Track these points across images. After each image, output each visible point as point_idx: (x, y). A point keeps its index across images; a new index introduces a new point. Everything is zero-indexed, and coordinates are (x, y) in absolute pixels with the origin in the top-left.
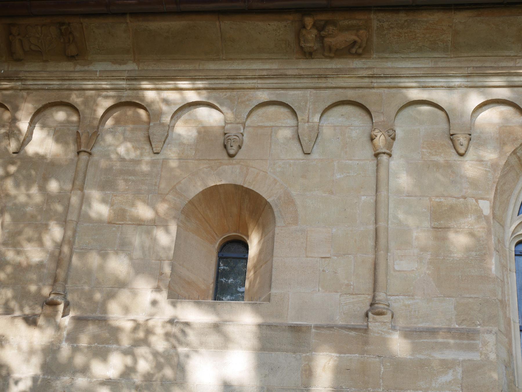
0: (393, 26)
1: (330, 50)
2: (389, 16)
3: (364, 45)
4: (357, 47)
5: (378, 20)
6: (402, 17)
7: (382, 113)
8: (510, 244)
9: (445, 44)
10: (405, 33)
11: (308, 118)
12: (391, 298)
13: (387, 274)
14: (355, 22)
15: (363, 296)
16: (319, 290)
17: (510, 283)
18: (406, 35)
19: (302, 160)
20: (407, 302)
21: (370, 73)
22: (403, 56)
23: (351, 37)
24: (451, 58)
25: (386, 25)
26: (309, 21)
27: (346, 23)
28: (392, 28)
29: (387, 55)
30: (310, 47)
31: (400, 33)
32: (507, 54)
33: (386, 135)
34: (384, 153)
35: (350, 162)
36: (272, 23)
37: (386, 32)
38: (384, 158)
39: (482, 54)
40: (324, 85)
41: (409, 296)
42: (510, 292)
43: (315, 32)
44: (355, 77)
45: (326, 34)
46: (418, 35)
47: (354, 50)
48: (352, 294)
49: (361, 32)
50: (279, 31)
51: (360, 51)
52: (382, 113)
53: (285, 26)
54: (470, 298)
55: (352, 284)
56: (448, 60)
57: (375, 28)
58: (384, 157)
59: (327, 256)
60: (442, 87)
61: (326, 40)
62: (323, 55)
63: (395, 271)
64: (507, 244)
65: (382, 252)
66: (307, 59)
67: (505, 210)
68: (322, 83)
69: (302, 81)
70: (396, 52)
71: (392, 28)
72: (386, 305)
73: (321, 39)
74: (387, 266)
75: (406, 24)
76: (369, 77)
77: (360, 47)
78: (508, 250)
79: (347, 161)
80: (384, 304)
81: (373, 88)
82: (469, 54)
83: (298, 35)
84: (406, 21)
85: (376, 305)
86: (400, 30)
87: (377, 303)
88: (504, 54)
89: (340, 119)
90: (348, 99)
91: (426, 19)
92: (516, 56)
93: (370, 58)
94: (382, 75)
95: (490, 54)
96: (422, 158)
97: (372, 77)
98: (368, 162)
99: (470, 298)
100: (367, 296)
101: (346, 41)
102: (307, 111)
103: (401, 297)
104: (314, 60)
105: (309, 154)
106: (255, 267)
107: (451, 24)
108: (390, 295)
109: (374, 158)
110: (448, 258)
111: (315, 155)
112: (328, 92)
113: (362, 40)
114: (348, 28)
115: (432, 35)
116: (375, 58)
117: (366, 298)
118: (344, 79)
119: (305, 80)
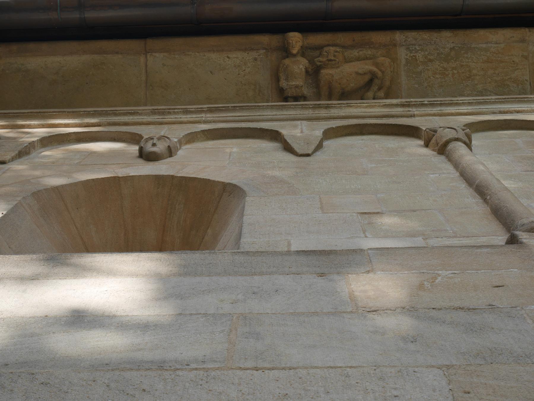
0: (432, 57)
2: (425, 35)
3: (388, 83)
5: (408, 49)
6: (447, 39)
9: (520, 87)
10: (453, 68)
14: (369, 52)
18: (455, 72)
25: (420, 56)
28: (431, 61)
30: (297, 87)
31: (445, 69)
36: (233, 55)
37: (421, 68)
45: (324, 59)
46: (474, 72)
50: (244, 68)
53: (255, 59)
57: (403, 62)
61: (325, 72)
71: (431, 61)
73: (314, 73)
75: (453, 53)
77: (380, 89)
86: (445, 65)
91: (484, 46)
101: (357, 73)
105: (308, 155)
106: (67, 150)
107: (525, 54)
113: (383, 72)
115: (497, 72)
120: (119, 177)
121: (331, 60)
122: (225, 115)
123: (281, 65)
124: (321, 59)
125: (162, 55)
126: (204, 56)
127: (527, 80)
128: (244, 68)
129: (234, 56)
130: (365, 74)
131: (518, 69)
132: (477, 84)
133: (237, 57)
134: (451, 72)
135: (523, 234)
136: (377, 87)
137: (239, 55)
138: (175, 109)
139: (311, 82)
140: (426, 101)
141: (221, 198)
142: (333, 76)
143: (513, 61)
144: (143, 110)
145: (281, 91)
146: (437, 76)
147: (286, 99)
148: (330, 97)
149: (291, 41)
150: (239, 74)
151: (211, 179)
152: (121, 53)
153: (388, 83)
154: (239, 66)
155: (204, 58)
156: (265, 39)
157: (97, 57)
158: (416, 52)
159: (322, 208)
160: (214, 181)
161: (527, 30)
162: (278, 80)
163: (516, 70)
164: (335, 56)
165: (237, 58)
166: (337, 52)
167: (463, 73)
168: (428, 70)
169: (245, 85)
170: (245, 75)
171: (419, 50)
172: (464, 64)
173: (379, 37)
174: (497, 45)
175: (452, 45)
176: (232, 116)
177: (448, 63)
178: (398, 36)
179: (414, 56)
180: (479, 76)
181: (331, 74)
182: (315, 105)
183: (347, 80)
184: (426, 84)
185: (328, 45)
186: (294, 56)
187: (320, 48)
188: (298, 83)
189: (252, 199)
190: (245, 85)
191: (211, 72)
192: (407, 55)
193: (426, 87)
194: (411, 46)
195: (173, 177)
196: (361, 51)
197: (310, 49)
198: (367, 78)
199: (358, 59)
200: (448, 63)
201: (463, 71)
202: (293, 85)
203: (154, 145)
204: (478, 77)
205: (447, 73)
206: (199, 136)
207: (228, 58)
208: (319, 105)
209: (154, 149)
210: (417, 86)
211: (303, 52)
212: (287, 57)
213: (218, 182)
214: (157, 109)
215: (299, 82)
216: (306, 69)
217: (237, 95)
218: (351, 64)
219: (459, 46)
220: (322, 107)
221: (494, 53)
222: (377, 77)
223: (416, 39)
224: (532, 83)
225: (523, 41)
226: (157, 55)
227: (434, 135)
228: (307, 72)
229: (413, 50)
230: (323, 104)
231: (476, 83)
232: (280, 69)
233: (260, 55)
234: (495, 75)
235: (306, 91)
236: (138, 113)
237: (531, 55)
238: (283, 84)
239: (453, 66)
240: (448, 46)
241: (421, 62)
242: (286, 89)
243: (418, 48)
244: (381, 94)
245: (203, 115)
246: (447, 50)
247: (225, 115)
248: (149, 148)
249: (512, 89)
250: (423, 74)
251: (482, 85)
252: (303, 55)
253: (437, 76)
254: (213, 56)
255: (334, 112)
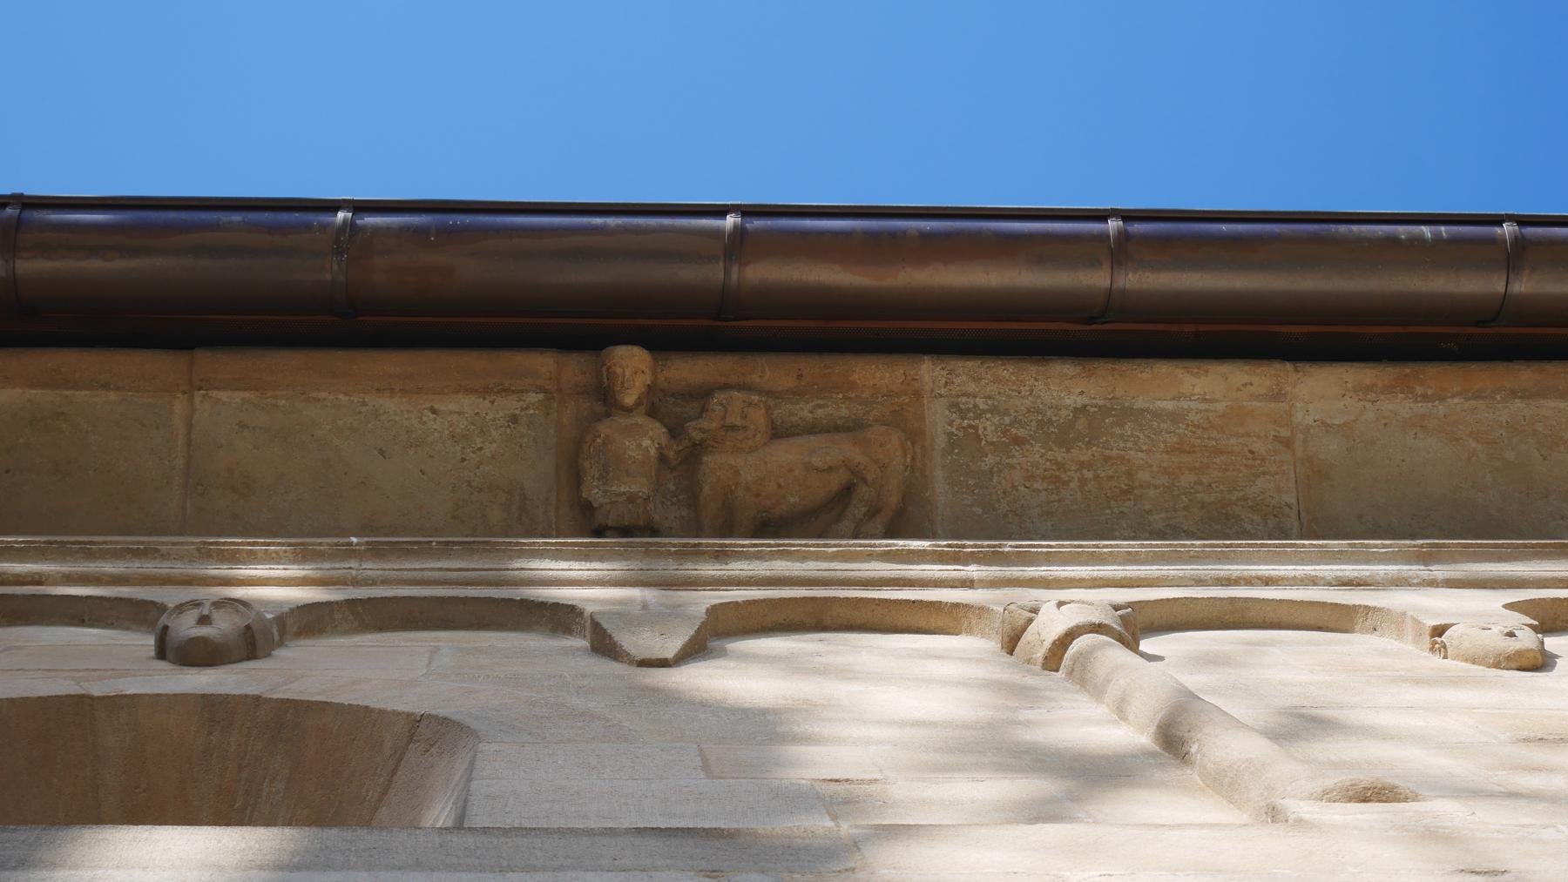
0: (1022, 433)
5: (954, 406)
10: (1082, 465)
18: (1089, 475)
30: (632, 499)
31: (1061, 466)
36: (448, 405)
37: (990, 460)
46: (1143, 476)
50: (478, 442)
53: (514, 419)
57: (941, 442)
71: (1018, 441)
73: (684, 461)
86: (1060, 454)
91: (1169, 405)
101: (809, 467)
107: (1285, 433)
120: (90, 697)
121: (733, 428)
122: (417, 565)
123: (589, 438)
124: (705, 424)
125: (239, 396)
126: (364, 404)
127: (1289, 506)
128: (478, 442)
129: (452, 407)
130: (830, 469)
131: (1264, 473)
133: (460, 409)
134: (1076, 476)
135: (1301, 804)
136: (864, 510)
137: (467, 403)
138: (268, 544)
140: (1008, 546)
141: (400, 760)
142: (737, 472)
143: (1252, 452)
144: (174, 544)
145: (587, 508)
147: (598, 533)
148: (728, 530)
149: (619, 370)
150: (463, 460)
151: (372, 705)
152: (117, 389)
154: (464, 437)
155: (364, 409)
156: (543, 363)
157: (45, 397)
158: (979, 417)
159: (706, 767)
160: (382, 712)
161: (1289, 366)
162: (577, 478)
163: (1257, 476)
165: (459, 413)
167: (1110, 478)
168: (1012, 467)
169: (480, 490)
170: (481, 463)
171: (985, 412)
172: (1114, 453)
174: (1204, 406)
175: (1080, 401)
176: (440, 569)
177: (1068, 451)
178: (929, 371)
179: (970, 426)
180: (1156, 487)
182: (685, 545)
183: (779, 485)
184: (1004, 507)
185: (726, 387)
186: (629, 410)
187: (703, 394)
188: (635, 488)
189: (497, 747)
190: (480, 490)
191: (381, 452)
192: (951, 423)
193: (1005, 515)
194: (964, 399)
195: (257, 699)
196: (819, 406)
197: (673, 395)
198: (836, 481)
199: (812, 429)
200: (1068, 451)
201: (1110, 473)
202: (620, 495)
203: (204, 620)
204: (1152, 492)
205: (1065, 477)
206: (338, 616)
207: (434, 411)
208: (695, 545)
209: (204, 631)
210: (979, 511)
211: (654, 404)
212: (608, 415)
213: (395, 713)
214: (217, 544)
216: (660, 449)
217: (454, 517)
218: (792, 440)
219: (1101, 403)
220: (703, 553)
222: (864, 480)
223: (977, 380)
224: (1303, 514)
225: (1277, 396)
226: (224, 396)
227: (1030, 621)
228: (662, 459)
229: (968, 410)
230: (708, 545)
231: (1147, 507)
232: (586, 448)
233: (527, 408)
234: (1200, 488)
236: (157, 550)
237: (1300, 436)
238: (594, 492)
239: (1082, 459)
240: (1068, 402)
241: (992, 443)
242: (601, 506)
243: (982, 406)
244: (879, 523)
245: (354, 564)
247: (417, 565)
248: (186, 627)
250: (995, 479)
251: (1163, 515)
252: (653, 413)
253: (1037, 485)
254: (391, 404)
255: (738, 568)
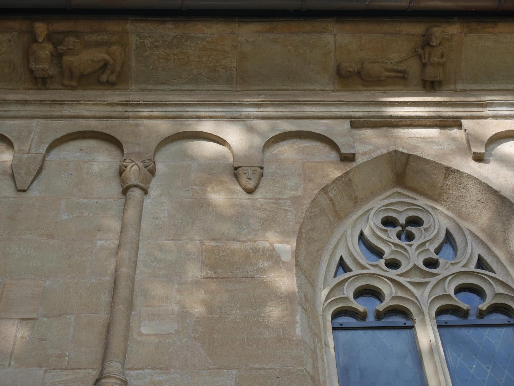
0: (157, 44)
1: (71, 76)
3: (118, 69)
4: (109, 72)
5: (138, 35)
6: (169, 30)
7: (138, 144)
8: (325, 310)
10: (175, 55)
11: (30, 149)
12: (132, 372)
13: (126, 338)
14: (106, 37)
15: (83, 370)
16: (10, 365)
17: (325, 360)
18: (176, 57)
19: (13, 198)
20: (156, 379)
21: (125, 99)
22: (172, 88)
23: (99, 55)
24: (237, 91)
25: (148, 42)
26: (41, 28)
27: (94, 38)
28: (156, 47)
29: (150, 87)
30: (43, 70)
31: (168, 55)
32: (312, 88)
33: (142, 168)
34: (136, 186)
35: (85, 200)
37: (148, 53)
38: (136, 193)
39: (278, 88)
40: (58, 114)
41: (161, 369)
42: (327, 372)
43: (49, 47)
44: (103, 104)
45: (65, 48)
47: (105, 77)
48: (66, 369)
49: (114, 48)
51: (113, 78)
52: (138, 144)
54: (262, 369)
55: (67, 354)
56: (233, 93)
57: (134, 47)
58: (136, 193)
59: (32, 317)
60: (224, 117)
61: (65, 58)
62: (63, 84)
63: (140, 334)
64: (321, 309)
65: (121, 306)
66: (39, 89)
67: (316, 264)
68: (56, 111)
69: (27, 108)
70: (163, 83)
71: (156, 47)
72: (121, 380)
73: (58, 57)
74: (128, 327)
75: (175, 41)
76: (122, 104)
77: (112, 72)
78: (321, 317)
79: (81, 200)
80: (116, 378)
81: (128, 118)
82: (261, 87)
83: (27, 55)
84: (175, 37)
85: (104, 380)
86: (168, 51)
87: (105, 377)
88: (307, 88)
89: (77, 154)
90: (91, 129)
91: (201, 35)
92: (323, 90)
93: (127, 89)
94: (141, 102)
95: (288, 88)
96: (192, 195)
97: (127, 105)
98: (113, 200)
99: (262, 369)
100: (90, 371)
101: (93, 61)
102: (30, 142)
103: (147, 371)
104: (49, 91)
105: (24, 191)
107: (235, 44)
108: (129, 369)
109: (121, 196)
110: (226, 316)
111: (34, 192)
112: (63, 122)
113: (114, 60)
114: (97, 44)
116: (134, 89)
117: (89, 373)
118: (86, 107)
119: (32, 108)
121: (71, 49)
127: (234, 67)
132: (193, 69)
139: (56, 62)
146: (161, 61)
153: (118, 69)
156: (16, 25)
158: (145, 39)
162: (28, 61)
163: (225, 58)
164: (74, 46)
166: (75, 42)
168: (154, 55)
171: (147, 37)
172: (184, 51)
173: (113, 26)
175: (175, 34)
177: (171, 50)
179: (143, 42)
180: (195, 62)
181: (71, 61)
184: (151, 67)
192: (137, 41)
196: (98, 35)
198: (101, 64)
200: (171, 50)
201: (182, 57)
204: (194, 63)
205: (169, 58)
215: (45, 66)
221: (209, 42)
229: (142, 37)
235: (52, 72)
238: (33, 66)
240: (171, 34)
241: (149, 47)
246: (170, 38)
249: (221, 74)
253: (161, 61)
